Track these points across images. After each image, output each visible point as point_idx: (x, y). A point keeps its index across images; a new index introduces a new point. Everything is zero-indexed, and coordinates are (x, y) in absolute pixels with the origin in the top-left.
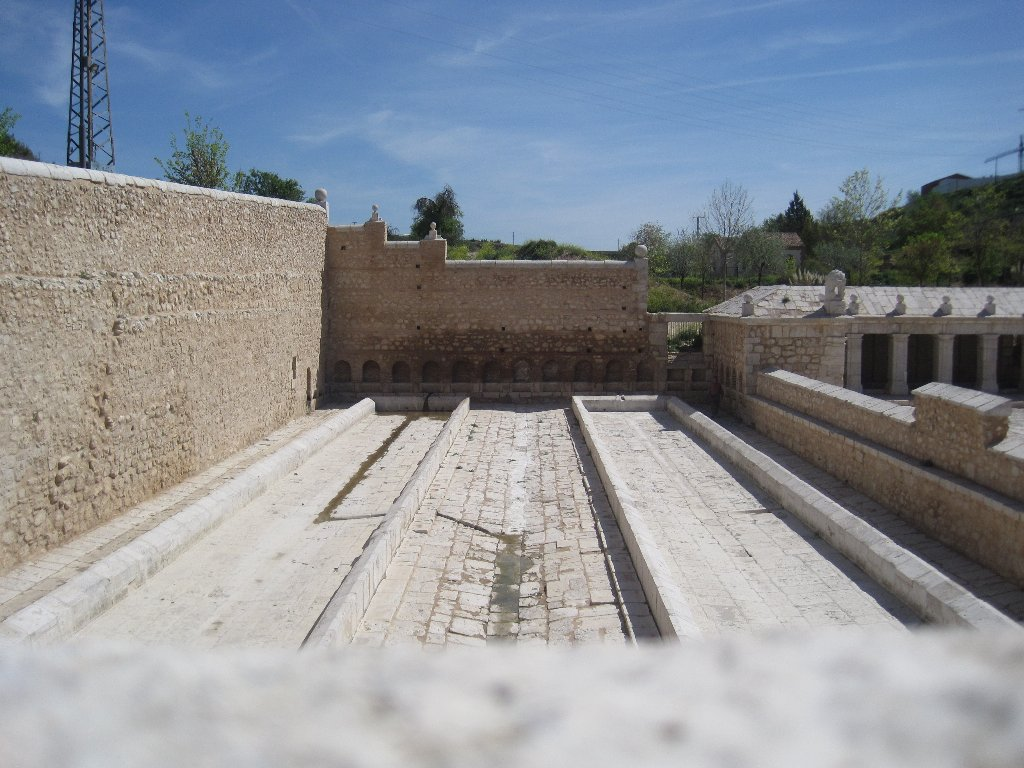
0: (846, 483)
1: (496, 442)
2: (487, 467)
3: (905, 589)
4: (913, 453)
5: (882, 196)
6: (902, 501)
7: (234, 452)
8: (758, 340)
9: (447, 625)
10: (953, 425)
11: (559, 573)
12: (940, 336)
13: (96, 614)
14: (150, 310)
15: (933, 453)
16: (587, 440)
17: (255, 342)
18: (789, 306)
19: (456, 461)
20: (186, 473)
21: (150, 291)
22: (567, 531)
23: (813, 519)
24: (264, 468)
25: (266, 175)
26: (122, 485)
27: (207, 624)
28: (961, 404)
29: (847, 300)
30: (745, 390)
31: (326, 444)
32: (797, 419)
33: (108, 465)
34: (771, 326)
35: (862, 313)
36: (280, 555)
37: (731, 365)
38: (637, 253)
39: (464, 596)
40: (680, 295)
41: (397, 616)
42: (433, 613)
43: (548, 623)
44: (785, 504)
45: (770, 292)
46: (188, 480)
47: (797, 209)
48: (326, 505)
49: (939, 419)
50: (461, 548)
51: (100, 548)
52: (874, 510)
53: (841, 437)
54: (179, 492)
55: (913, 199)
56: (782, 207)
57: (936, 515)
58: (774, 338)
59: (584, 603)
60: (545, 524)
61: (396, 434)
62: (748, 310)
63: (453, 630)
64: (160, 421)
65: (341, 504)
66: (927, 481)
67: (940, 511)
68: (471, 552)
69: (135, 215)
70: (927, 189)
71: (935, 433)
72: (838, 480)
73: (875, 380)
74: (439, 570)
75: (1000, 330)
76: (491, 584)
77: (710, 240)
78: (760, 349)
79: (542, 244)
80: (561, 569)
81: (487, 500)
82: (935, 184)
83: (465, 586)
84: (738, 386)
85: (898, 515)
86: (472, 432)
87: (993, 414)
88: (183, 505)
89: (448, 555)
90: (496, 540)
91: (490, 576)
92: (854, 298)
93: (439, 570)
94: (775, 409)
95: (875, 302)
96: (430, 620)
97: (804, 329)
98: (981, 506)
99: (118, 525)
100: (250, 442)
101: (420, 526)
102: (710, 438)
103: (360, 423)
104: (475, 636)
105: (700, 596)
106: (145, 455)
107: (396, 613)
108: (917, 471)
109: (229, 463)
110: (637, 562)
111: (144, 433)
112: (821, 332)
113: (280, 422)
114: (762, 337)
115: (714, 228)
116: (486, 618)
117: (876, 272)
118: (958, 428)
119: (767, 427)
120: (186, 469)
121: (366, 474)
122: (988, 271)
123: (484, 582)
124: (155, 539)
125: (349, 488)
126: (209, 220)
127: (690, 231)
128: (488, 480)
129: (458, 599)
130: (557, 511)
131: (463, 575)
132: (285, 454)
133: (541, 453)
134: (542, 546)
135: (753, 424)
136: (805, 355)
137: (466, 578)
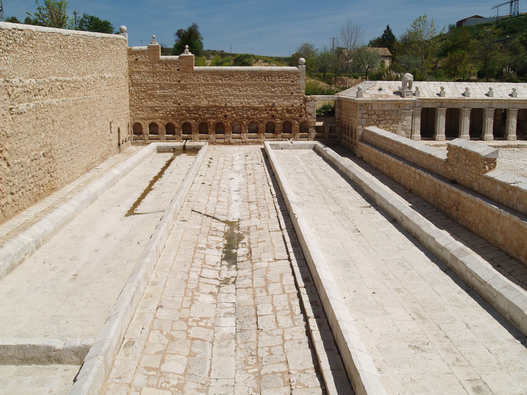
0: (411, 191)
1: (223, 168)
2: (218, 183)
3: (440, 251)
4: (446, 176)
5: (434, 30)
6: (440, 201)
7: (79, 176)
8: (365, 111)
9: (199, 273)
10: (468, 162)
11: (258, 242)
12: (463, 109)
13: (8, 272)
14: (30, 101)
15: (456, 176)
16: (272, 167)
17: (89, 115)
18: (382, 93)
19: (201, 179)
20: (53, 189)
21: (29, 89)
22: (262, 219)
23: (392, 211)
24: (97, 185)
25: (92, 18)
26: (18, 198)
27: (70, 276)
28: (472, 151)
29: (413, 89)
30: (358, 139)
31: (130, 170)
32: (385, 155)
33: (9, 187)
34: (372, 104)
35: (421, 96)
36: (108, 235)
37: (350, 125)
38: (299, 63)
39: (207, 257)
40: (322, 85)
41: (173, 269)
42: (191, 267)
43: (253, 271)
44: (378, 203)
45: (372, 85)
46: (54, 193)
47: (388, 34)
48: (132, 206)
49: (460, 158)
50: (205, 229)
51: (7, 234)
52: (425, 206)
53: (408, 166)
54: (49, 201)
55: (451, 28)
56: (379, 33)
57: (457, 210)
58: (374, 111)
59: (271, 259)
60: (250, 215)
61: (168, 164)
62: (359, 93)
63: (202, 275)
64: (38, 162)
65: (139, 205)
66: (453, 192)
67: (459, 208)
68: (211, 232)
69: (18, 46)
70: (460, 23)
71: (458, 166)
72: (407, 189)
73: (428, 133)
74: (194, 242)
75: (496, 106)
76: (222, 249)
77: (339, 51)
78: (366, 116)
79: (247, 56)
80: (259, 241)
81: (218, 201)
82: (465, 20)
83: (208, 251)
84: (354, 136)
85: (438, 209)
86: (210, 162)
87: (489, 157)
88: (52, 208)
89: (198, 233)
90: (224, 224)
91: (221, 245)
92: (417, 88)
93: (194, 242)
94: (374, 150)
95: (429, 90)
96: (190, 271)
97: (390, 105)
98: (480, 205)
99: (16, 220)
100: (88, 171)
101: (183, 218)
102: (338, 165)
103: (146, 156)
104: (214, 279)
105: (333, 255)
106: (30, 181)
107: (171, 267)
108: (448, 186)
109: (77, 182)
110: (300, 239)
111: (29, 169)
112: (399, 107)
113: (103, 159)
114: (368, 110)
115: (342, 45)
116: (220, 268)
117: (430, 71)
118: (470, 164)
119: (369, 159)
120: (53, 187)
121: (152, 187)
122: (491, 72)
123: (218, 248)
124: (37, 230)
125: (143, 196)
126: (61, 46)
127: (329, 47)
128: (219, 190)
129: (204, 258)
130: (256, 207)
131: (207, 245)
132: (108, 177)
133: (247, 175)
134: (249, 228)
135: (362, 157)
136: (390, 119)
137: (209, 246)
